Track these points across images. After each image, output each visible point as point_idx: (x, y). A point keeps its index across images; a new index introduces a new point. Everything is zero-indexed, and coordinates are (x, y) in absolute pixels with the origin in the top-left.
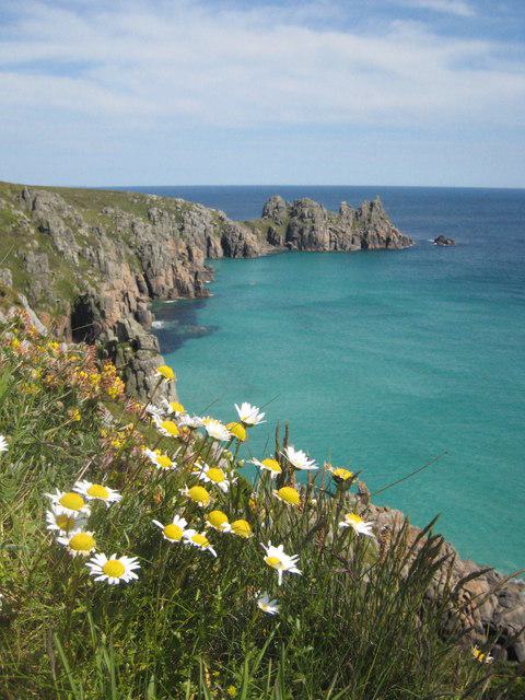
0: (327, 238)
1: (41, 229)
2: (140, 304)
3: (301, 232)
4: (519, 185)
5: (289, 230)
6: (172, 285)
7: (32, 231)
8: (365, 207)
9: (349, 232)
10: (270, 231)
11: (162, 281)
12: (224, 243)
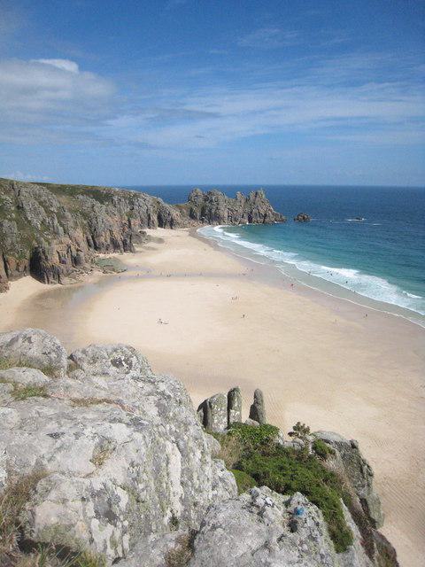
1: (18, 207)
2: (79, 253)
3: (210, 211)
4: (420, 184)
5: (203, 210)
6: (109, 241)
7: (13, 208)
8: (252, 195)
9: (240, 211)
10: (191, 210)
11: (102, 239)
12: (159, 218)
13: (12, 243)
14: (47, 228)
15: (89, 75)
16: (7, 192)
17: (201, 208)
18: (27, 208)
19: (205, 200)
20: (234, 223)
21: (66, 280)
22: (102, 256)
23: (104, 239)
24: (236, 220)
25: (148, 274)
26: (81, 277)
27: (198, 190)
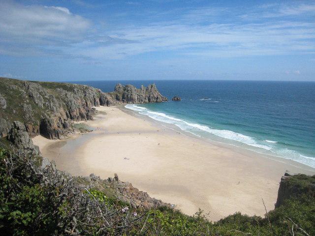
0: (136, 98)
1: (30, 96)
2: (65, 121)
4: (310, 79)
6: (78, 114)
7: (27, 97)
9: (144, 95)
10: (117, 96)
11: (75, 113)
12: (100, 100)
13: (30, 117)
14: (47, 108)
15: (78, 17)
16: (22, 87)
17: (122, 94)
18: (35, 97)
19: (124, 90)
20: (141, 102)
21: (62, 137)
22: (75, 122)
23: (76, 113)
24: (142, 101)
25: (104, 132)
26: (69, 135)
27: (120, 84)
